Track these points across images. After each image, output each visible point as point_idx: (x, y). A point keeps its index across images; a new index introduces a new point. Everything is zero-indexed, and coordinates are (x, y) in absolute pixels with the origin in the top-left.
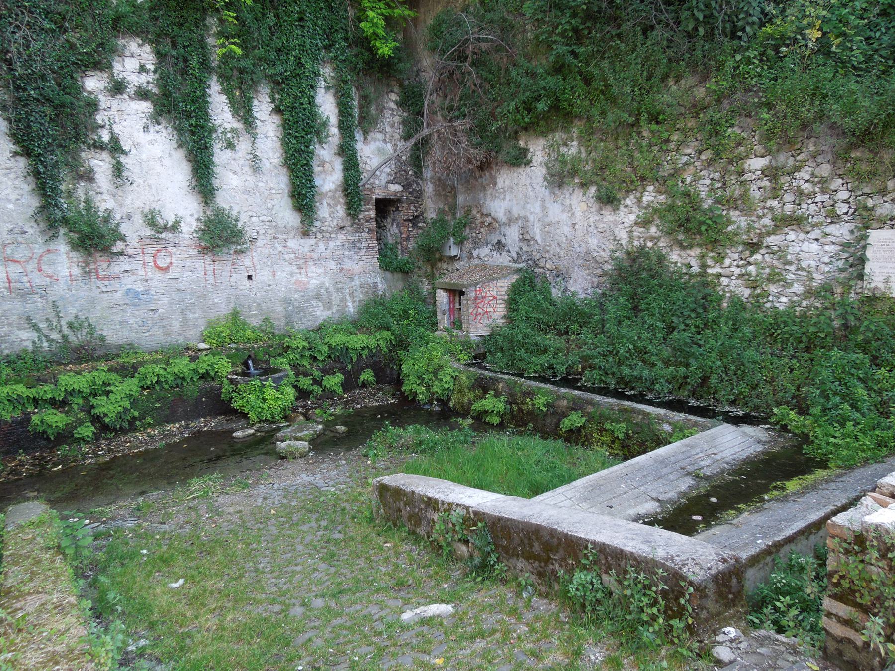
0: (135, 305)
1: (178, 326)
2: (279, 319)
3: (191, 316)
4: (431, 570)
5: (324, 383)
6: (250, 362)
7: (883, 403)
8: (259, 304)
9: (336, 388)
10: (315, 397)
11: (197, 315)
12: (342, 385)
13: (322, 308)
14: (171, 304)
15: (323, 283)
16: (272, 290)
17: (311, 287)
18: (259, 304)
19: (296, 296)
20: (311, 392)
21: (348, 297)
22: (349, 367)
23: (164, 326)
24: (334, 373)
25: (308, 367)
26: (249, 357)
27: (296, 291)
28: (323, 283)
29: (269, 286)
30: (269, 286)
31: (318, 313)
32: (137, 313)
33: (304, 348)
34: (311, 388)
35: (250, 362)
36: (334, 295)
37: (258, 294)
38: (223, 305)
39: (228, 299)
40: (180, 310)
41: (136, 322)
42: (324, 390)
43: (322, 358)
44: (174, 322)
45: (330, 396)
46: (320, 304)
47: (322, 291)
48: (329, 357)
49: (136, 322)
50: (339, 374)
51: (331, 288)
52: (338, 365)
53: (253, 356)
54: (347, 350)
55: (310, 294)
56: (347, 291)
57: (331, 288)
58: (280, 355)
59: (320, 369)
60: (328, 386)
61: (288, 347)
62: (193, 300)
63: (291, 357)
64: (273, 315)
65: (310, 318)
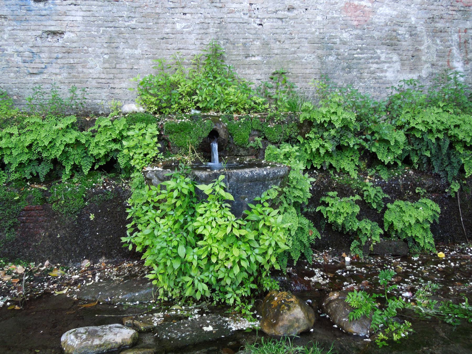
0: (18, 19)
1: (99, 68)
2: (305, 78)
3: (128, 51)
4: (365, 188)
5: (389, 217)
6: (215, 146)
7: (230, 246)
8: (266, 44)
9: (417, 232)
10: (365, 248)
11: (138, 52)
12: (434, 228)
13: (397, 66)
14: (88, 24)
15: (405, 16)
16: (294, 18)
17: (381, 21)
18: (266, 44)
19: (345, 36)
20: (356, 234)
21: (455, 50)
22: (456, 187)
23: (72, 66)
24: (415, 198)
25: (354, 175)
26: (214, 134)
27: (346, 26)
28: (405, 16)
29: (290, 9)
30: (290, 9)
31: (390, 75)
32: (21, 34)
33: (345, 127)
34: (356, 225)
35: (215, 146)
36: (427, 41)
37: (267, 24)
38: (193, 37)
39: (204, 25)
40: (105, 39)
41: (19, 53)
42: (386, 235)
43: (388, 159)
44: (92, 62)
45: (402, 250)
46: (395, 57)
47: (401, 31)
48: (407, 161)
49: (19, 53)
50: (429, 202)
51: (421, 28)
52: (428, 182)
53: (222, 133)
54: (451, 147)
55: (376, 34)
56: (455, 37)
57: (421, 28)
58: (290, 140)
59: (382, 185)
60: (399, 226)
61: (310, 123)
62: (133, 23)
63: (314, 145)
64: (295, 69)
65: (372, 83)
